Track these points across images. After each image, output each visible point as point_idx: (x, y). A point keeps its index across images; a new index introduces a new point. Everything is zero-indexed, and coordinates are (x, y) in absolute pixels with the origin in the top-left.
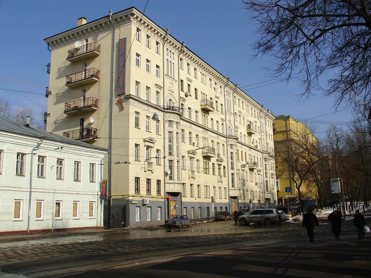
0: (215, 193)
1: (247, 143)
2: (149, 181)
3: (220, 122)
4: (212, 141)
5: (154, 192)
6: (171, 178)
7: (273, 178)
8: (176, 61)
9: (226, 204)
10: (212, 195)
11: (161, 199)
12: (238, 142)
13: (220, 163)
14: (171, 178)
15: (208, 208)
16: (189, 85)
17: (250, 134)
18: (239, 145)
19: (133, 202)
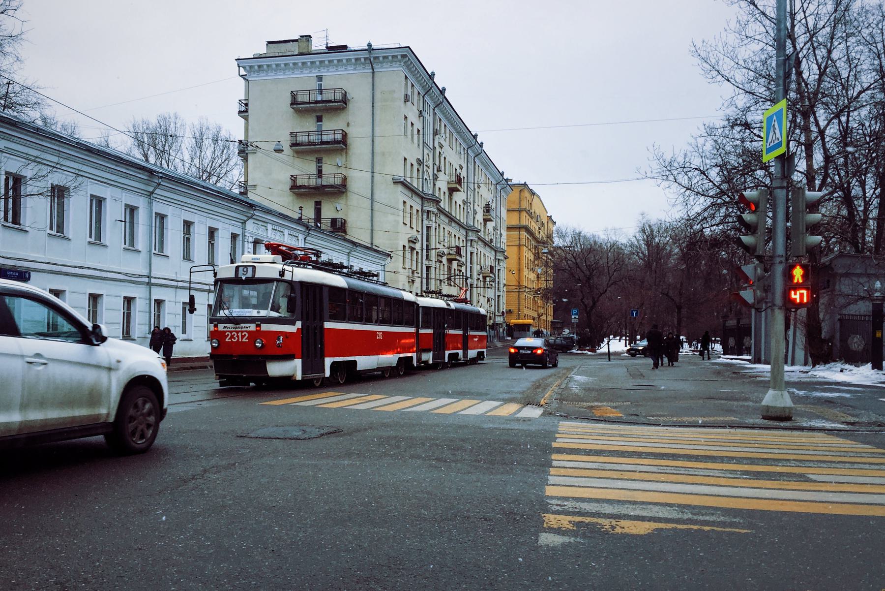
3: (416, 167)
17: (452, 191)
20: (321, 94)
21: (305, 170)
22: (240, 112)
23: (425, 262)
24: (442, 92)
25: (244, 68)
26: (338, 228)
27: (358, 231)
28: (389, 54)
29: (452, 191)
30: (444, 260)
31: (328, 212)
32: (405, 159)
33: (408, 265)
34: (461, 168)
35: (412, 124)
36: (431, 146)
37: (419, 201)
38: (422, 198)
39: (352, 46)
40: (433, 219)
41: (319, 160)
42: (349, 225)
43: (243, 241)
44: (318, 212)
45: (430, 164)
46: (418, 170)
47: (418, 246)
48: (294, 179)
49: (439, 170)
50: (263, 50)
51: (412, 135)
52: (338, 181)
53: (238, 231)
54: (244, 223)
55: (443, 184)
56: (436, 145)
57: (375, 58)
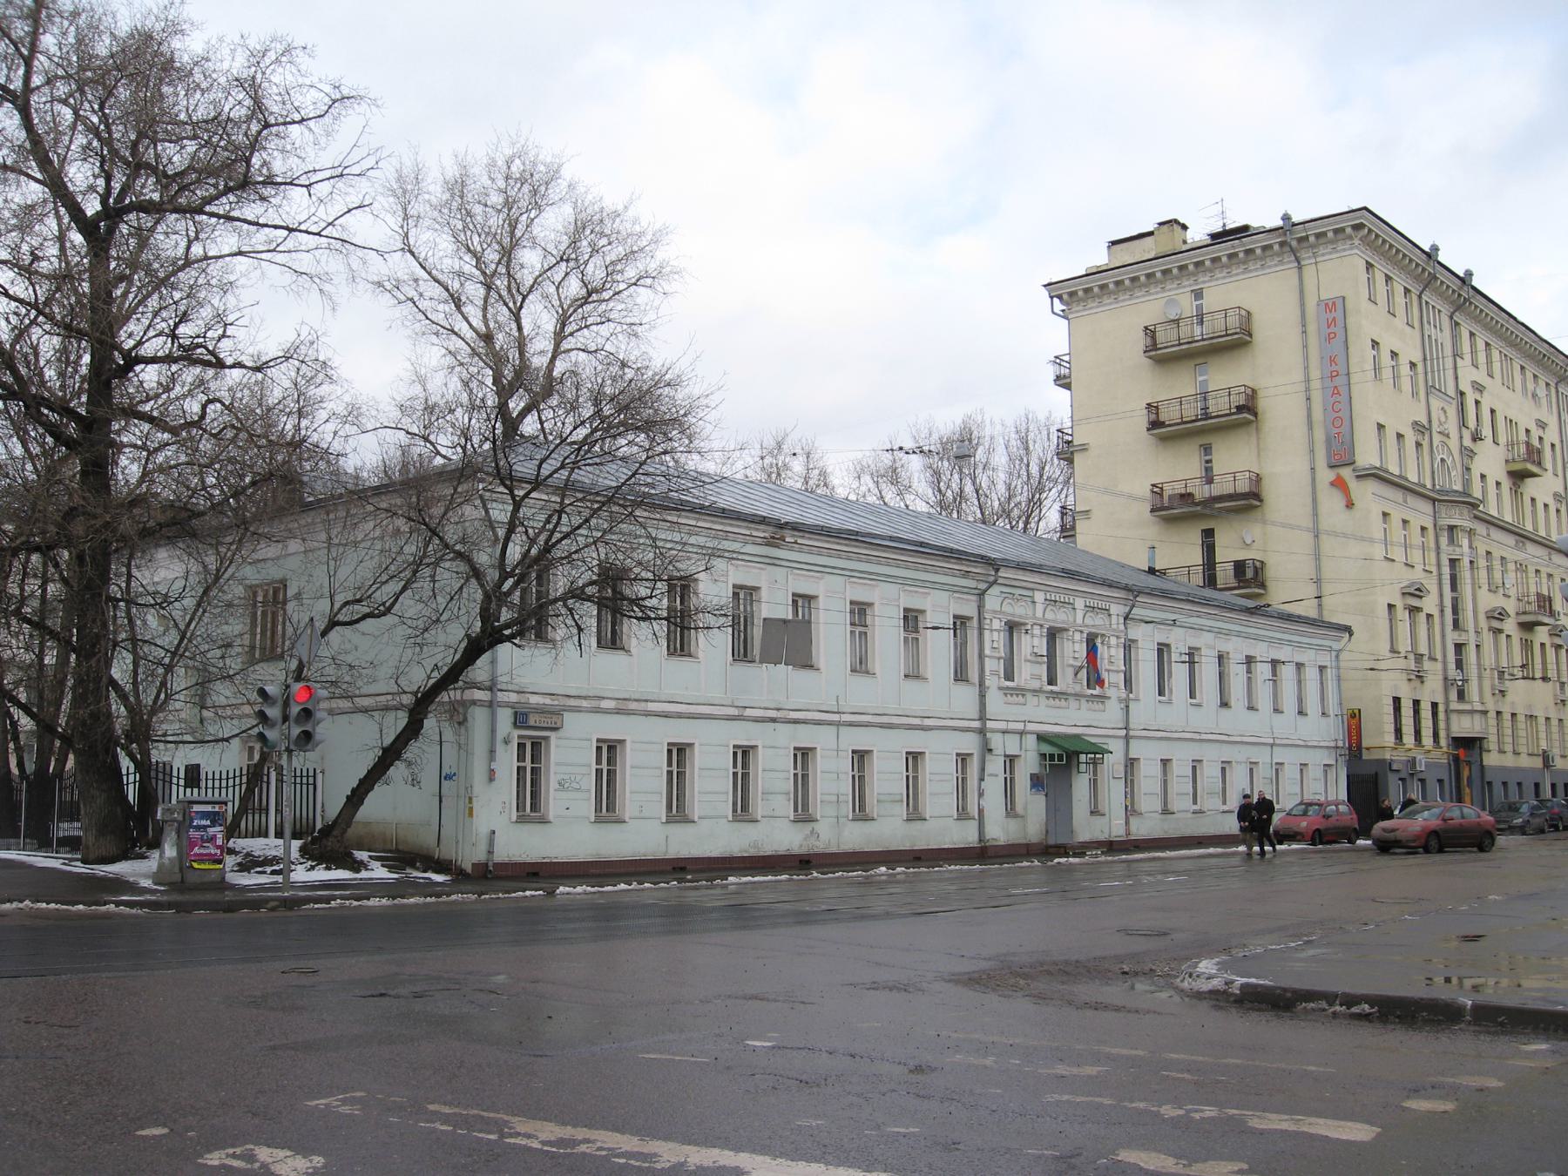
0: (1549, 739)
1: (1508, 518)
2: (1416, 703)
3: (1410, 438)
4: (1405, 522)
5: (1427, 740)
6: (1461, 696)
7: (1500, 631)
8: (1445, 337)
9: (1533, 770)
10: (1544, 745)
11: (1441, 756)
12: (1476, 517)
13: (1415, 602)
14: (1461, 696)
15: (1537, 785)
16: (1477, 402)
17: (1519, 476)
18: (1481, 529)
19: (1395, 767)
20: (1202, 322)
21: (1179, 469)
22: (1058, 378)
23: (1452, 637)
24: (1465, 280)
25: (1060, 297)
26: (1250, 576)
27: (1288, 586)
28: (1328, 227)
29: (1519, 476)
30: (1510, 626)
31: (1228, 552)
32: (1380, 427)
33: (1404, 645)
34: (1542, 425)
35: (1394, 354)
36: (1451, 391)
37: (1427, 507)
38: (1434, 500)
39: (1255, 223)
40: (1465, 542)
41: (1207, 449)
42: (1271, 573)
43: (981, 630)
44: (1209, 549)
45: (1452, 426)
46: (1418, 445)
47: (1429, 604)
48: (1157, 490)
49: (1476, 438)
50: (1101, 258)
51: (1396, 378)
52: (1243, 486)
53: (969, 609)
54: (981, 595)
55: (1491, 462)
56: (1465, 386)
57: (1300, 240)
